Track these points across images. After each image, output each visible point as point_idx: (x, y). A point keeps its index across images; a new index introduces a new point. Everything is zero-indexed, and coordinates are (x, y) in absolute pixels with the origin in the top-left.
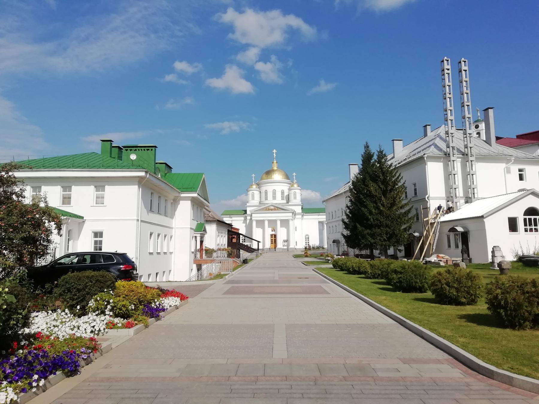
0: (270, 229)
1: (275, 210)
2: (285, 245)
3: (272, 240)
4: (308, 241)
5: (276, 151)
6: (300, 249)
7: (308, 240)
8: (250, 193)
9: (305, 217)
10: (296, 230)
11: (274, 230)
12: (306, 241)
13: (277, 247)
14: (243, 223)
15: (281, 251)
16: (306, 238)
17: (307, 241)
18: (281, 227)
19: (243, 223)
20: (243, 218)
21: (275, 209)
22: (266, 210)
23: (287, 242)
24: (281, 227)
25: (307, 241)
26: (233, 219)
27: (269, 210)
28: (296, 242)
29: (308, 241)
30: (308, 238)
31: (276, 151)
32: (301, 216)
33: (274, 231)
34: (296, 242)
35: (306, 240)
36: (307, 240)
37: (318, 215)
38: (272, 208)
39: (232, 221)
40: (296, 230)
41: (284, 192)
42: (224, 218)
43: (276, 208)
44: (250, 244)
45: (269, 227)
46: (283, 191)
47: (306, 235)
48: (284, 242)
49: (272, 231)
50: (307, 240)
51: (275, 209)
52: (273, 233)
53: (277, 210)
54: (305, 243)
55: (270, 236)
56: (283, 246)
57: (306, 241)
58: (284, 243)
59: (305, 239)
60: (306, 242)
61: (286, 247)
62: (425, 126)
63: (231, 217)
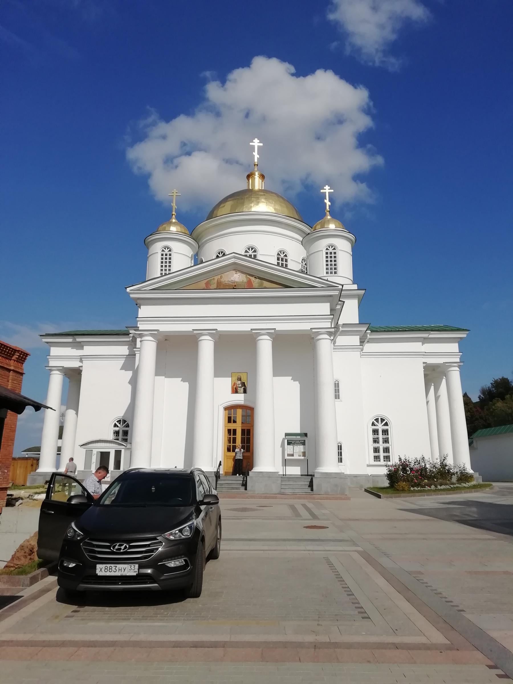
0: (227, 383)
1: (249, 286)
2: (296, 457)
3: (235, 431)
4: (386, 445)
5: (261, 144)
6: (356, 476)
7: (386, 441)
8: (157, 248)
9: (369, 347)
10: (337, 397)
11: (243, 384)
12: (376, 445)
13: (255, 469)
14: (125, 368)
15: (275, 489)
16: (375, 432)
17: (381, 446)
18: (277, 371)
19: (125, 368)
20: (124, 350)
21: (249, 282)
22: (207, 287)
23: (304, 443)
24: (277, 371)
25: (381, 446)
26: (88, 350)
27: (221, 286)
28: (340, 448)
29: (386, 445)
30: (385, 432)
31: (261, 144)
32: (355, 340)
33: (245, 392)
34: (340, 448)
35: (376, 441)
36: (381, 440)
37: (425, 340)
38: (237, 277)
39: (81, 361)
40: (337, 397)
41: (289, 258)
42: (388, 485)
43: (256, 282)
44: (119, 448)
45: (218, 372)
46: (282, 256)
47: (377, 420)
48: (289, 443)
49: (235, 391)
50: (381, 440)
51: (249, 282)
52: (239, 398)
53: (261, 287)
54: (372, 454)
55: (221, 417)
56: (285, 463)
57: (376, 445)
58: (289, 449)
59: (371, 436)
60: (376, 450)
61: (295, 471)
62: (361, 358)
63: (80, 346)
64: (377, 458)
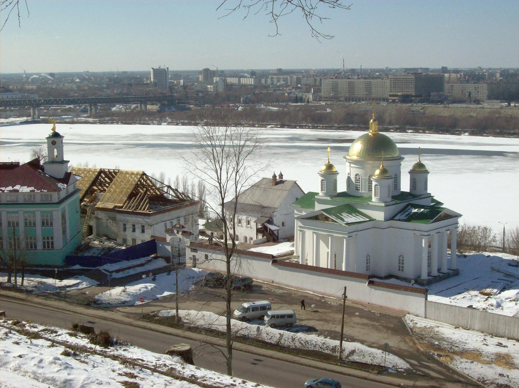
16: (400, 260)
64: (399, 270)
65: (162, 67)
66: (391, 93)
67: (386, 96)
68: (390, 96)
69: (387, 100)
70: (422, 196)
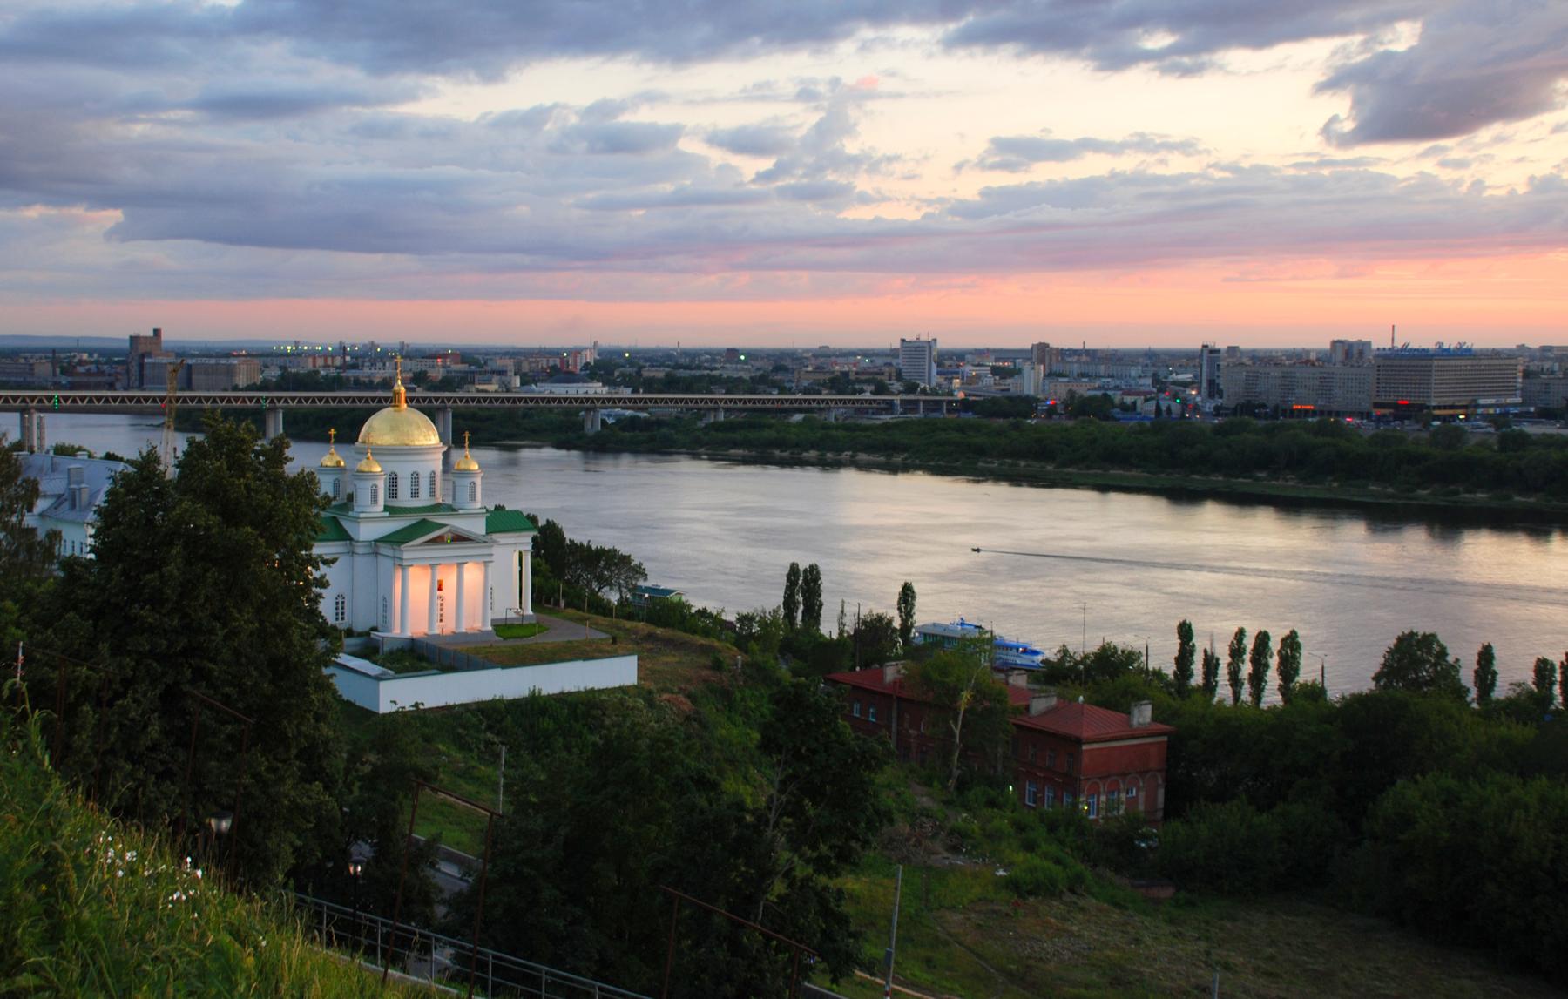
17: (340, 611)
65: (924, 338)
66: (1378, 400)
67: (1366, 406)
68: (1377, 405)
69: (1368, 415)
70: (461, 512)
